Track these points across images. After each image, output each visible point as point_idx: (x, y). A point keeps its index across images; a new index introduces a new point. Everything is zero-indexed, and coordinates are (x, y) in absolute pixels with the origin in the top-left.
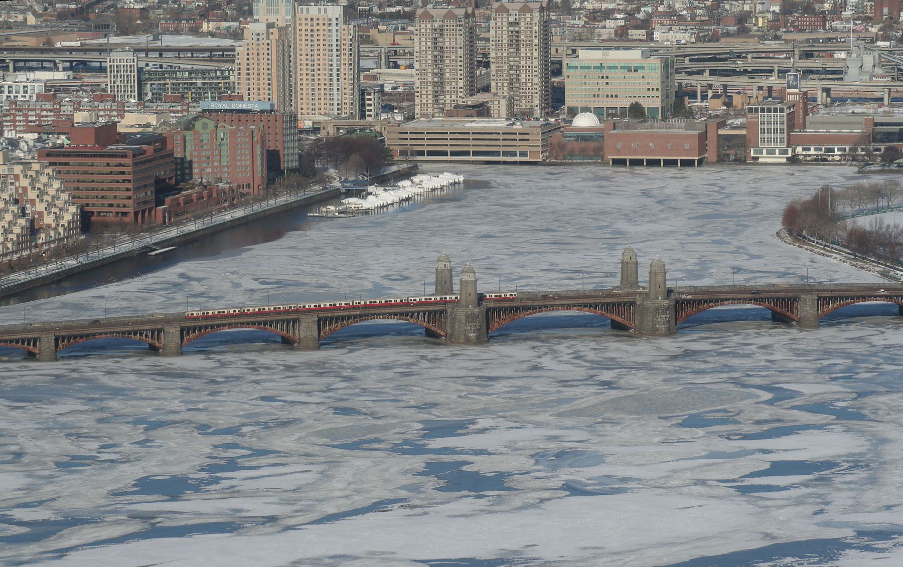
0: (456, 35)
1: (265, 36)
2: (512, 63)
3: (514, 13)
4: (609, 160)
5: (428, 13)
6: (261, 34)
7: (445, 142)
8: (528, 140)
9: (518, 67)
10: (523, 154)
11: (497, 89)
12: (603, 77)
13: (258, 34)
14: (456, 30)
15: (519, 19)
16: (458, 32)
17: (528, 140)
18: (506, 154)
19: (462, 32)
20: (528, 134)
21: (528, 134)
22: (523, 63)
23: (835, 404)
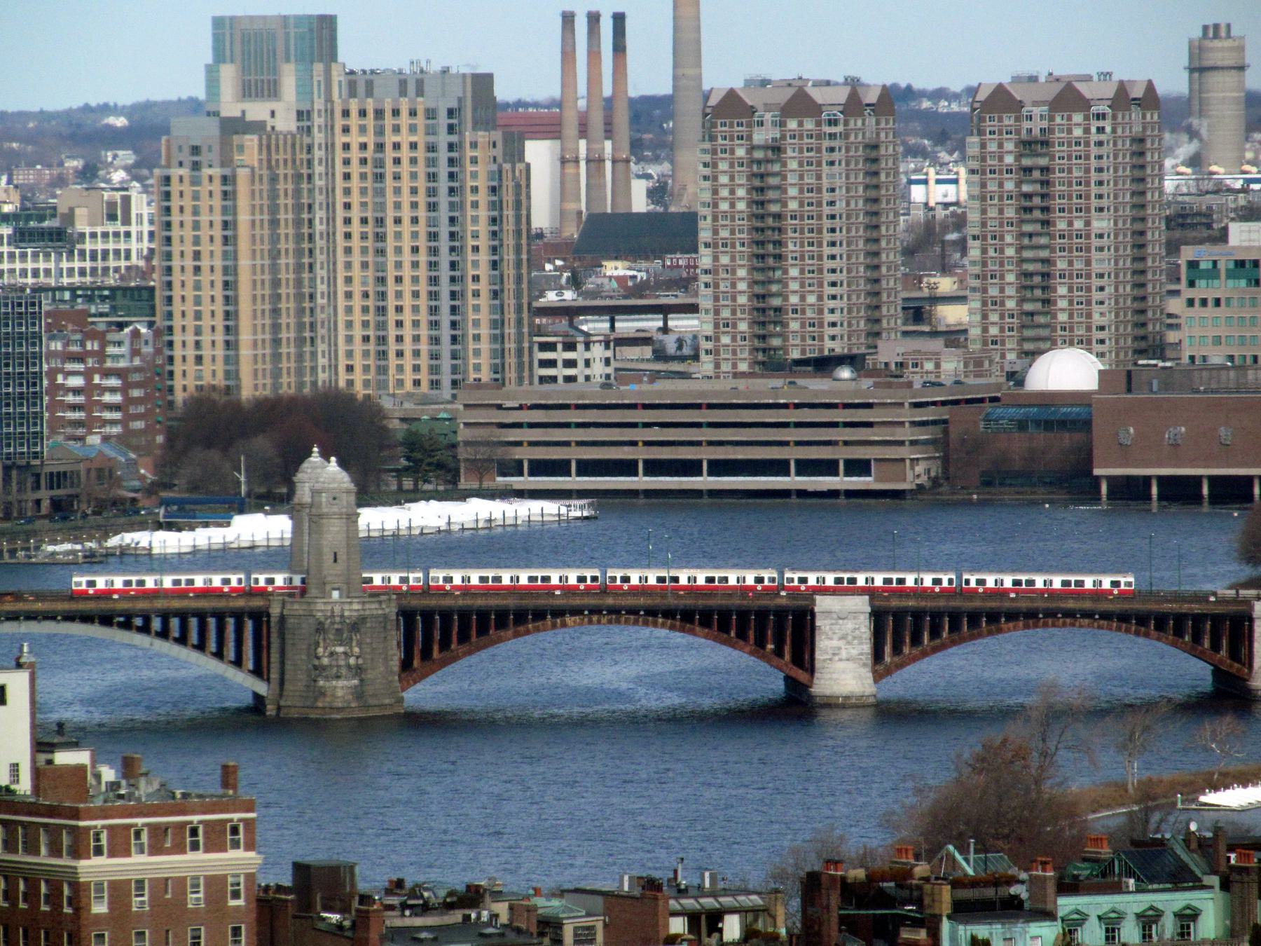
0: (819, 164)
1: (215, 156)
2: (1030, 267)
3: (1037, 111)
4: (1098, 478)
5: (807, 96)
6: (204, 149)
7: (628, 434)
8: (869, 425)
9: (1046, 276)
10: (858, 467)
11: (985, 343)
12: (1218, 302)
13: (196, 150)
14: (819, 150)
15: (1051, 131)
16: (826, 156)
17: (869, 425)
18: (806, 467)
19: (836, 156)
20: (869, 406)
21: (869, 406)
22: (1061, 265)
23: (577, 509)
